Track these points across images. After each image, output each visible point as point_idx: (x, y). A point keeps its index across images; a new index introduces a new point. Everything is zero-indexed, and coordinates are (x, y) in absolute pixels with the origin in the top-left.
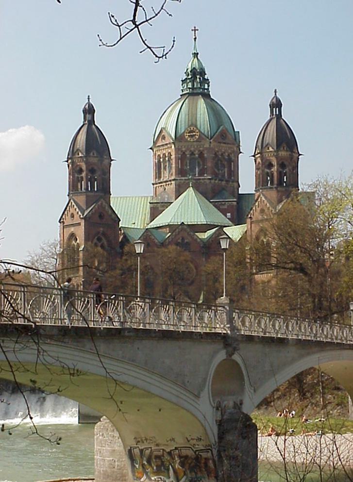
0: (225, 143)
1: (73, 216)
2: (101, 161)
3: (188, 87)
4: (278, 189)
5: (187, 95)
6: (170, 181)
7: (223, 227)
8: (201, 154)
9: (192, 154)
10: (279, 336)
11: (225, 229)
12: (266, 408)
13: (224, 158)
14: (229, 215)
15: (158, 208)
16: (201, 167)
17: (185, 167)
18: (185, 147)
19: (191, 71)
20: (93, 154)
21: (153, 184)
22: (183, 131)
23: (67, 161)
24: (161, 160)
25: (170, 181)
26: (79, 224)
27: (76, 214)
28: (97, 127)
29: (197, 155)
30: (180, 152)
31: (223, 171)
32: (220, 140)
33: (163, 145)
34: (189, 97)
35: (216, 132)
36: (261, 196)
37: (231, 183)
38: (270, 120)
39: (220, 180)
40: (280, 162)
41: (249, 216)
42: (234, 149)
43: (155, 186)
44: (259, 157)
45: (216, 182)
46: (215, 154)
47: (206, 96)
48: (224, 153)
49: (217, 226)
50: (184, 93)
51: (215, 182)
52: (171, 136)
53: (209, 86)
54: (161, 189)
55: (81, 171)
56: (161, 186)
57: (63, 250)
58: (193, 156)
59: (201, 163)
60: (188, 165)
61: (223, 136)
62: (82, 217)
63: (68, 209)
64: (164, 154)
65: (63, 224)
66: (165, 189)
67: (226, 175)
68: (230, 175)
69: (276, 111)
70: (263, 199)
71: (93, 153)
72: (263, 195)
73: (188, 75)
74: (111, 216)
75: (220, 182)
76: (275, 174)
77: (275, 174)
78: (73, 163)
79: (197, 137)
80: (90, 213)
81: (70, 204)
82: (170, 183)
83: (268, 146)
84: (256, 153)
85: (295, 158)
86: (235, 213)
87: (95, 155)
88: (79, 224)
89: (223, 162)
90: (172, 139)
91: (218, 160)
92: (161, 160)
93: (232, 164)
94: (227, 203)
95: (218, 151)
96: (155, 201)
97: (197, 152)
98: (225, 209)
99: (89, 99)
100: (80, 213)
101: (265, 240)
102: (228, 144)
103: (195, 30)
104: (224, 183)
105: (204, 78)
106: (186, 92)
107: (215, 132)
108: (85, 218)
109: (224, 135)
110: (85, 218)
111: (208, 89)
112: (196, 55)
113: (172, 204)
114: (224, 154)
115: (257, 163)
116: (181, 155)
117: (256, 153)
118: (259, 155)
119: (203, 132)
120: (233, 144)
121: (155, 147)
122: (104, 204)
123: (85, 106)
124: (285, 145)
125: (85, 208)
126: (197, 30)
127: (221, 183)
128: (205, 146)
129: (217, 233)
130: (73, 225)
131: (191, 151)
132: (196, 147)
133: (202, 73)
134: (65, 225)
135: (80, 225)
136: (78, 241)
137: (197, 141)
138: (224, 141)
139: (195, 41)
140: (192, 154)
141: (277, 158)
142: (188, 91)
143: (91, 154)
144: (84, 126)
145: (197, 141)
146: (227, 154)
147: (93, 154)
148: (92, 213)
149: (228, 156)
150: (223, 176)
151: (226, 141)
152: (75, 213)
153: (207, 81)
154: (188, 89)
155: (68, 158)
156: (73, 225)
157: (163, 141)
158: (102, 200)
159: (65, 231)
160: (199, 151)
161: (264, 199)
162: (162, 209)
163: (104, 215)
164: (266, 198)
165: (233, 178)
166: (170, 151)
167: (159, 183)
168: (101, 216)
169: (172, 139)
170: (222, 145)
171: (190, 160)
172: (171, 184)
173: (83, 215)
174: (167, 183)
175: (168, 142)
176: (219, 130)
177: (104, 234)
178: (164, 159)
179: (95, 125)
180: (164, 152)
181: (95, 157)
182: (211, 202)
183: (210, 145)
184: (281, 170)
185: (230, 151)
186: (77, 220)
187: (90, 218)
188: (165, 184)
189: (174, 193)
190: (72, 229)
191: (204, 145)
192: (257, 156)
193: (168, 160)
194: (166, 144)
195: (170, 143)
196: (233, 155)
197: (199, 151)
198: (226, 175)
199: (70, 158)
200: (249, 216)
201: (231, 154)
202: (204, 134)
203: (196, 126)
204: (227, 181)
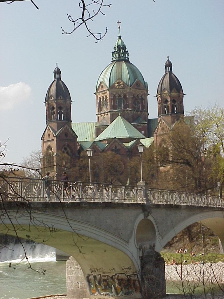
0: (139, 89)
1: (49, 135)
2: (65, 102)
3: (116, 56)
4: (172, 115)
6: (107, 112)
7: (139, 139)
8: (125, 96)
9: (120, 96)
10: (176, 204)
11: (141, 140)
13: (139, 98)
14: (143, 132)
15: (100, 129)
16: (125, 103)
18: (115, 92)
19: (117, 47)
20: (61, 98)
21: (97, 115)
22: (113, 83)
23: (45, 103)
25: (107, 112)
26: (53, 140)
29: (122, 97)
30: (112, 95)
32: (136, 87)
33: (102, 91)
35: (134, 83)
37: (143, 113)
39: (136, 111)
40: (172, 99)
41: (155, 132)
43: (98, 116)
44: (160, 96)
45: (135, 112)
46: (133, 96)
47: (127, 61)
49: (134, 139)
51: (134, 113)
52: (106, 86)
53: (128, 55)
54: (102, 118)
55: (53, 108)
56: (102, 116)
57: (44, 156)
58: (120, 97)
59: (125, 101)
60: (117, 102)
61: (138, 85)
62: (55, 136)
63: (46, 131)
64: (103, 97)
66: (104, 117)
67: (140, 108)
69: (169, 69)
70: (163, 121)
71: (61, 97)
72: (163, 119)
75: (137, 112)
76: (170, 106)
77: (170, 106)
78: (48, 104)
79: (122, 86)
81: (47, 128)
82: (107, 114)
84: (158, 94)
85: (181, 97)
86: (147, 131)
87: (62, 98)
88: (53, 140)
90: (107, 87)
92: (101, 100)
93: (144, 101)
94: (141, 125)
97: (122, 95)
99: (168, 58)
100: (53, 133)
101: (165, 146)
102: (141, 89)
103: (119, 23)
104: (139, 113)
105: (125, 51)
107: (133, 82)
108: (56, 137)
109: (138, 84)
110: (56, 137)
111: (128, 57)
112: (120, 37)
114: (139, 96)
116: (113, 97)
117: (158, 94)
118: (160, 95)
119: (126, 82)
120: (144, 89)
121: (97, 93)
122: (68, 127)
124: (175, 89)
125: (56, 131)
126: (120, 23)
128: (127, 91)
129: (136, 143)
130: (49, 141)
131: (119, 94)
132: (122, 91)
133: (124, 48)
134: (44, 141)
135: (54, 140)
136: (53, 150)
137: (122, 88)
138: (138, 88)
139: (119, 29)
140: (120, 96)
142: (116, 59)
143: (59, 98)
144: (55, 82)
145: (122, 88)
146: (140, 95)
147: (61, 98)
150: (139, 108)
152: (51, 134)
153: (127, 52)
154: (116, 58)
155: (45, 101)
156: (49, 141)
157: (102, 89)
158: (67, 125)
159: (44, 144)
160: (124, 94)
161: (164, 122)
162: (103, 129)
163: (68, 134)
164: (165, 121)
165: (144, 110)
166: (106, 95)
167: (101, 114)
168: (66, 135)
169: (107, 87)
170: (137, 90)
171: (119, 99)
172: (108, 114)
173: (55, 134)
174: (105, 114)
176: (135, 82)
177: (68, 145)
179: (61, 81)
180: (103, 95)
181: (62, 100)
182: (132, 124)
183: (130, 91)
187: (59, 136)
188: (104, 114)
190: (49, 143)
191: (127, 90)
192: (158, 96)
194: (104, 91)
195: (106, 90)
197: (124, 94)
198: (140, 108)
199: (47, 101)
200: (155, 132)
201: (143, 95)
202: (126, 84)
203: (121, 79)
204: (141, 112)
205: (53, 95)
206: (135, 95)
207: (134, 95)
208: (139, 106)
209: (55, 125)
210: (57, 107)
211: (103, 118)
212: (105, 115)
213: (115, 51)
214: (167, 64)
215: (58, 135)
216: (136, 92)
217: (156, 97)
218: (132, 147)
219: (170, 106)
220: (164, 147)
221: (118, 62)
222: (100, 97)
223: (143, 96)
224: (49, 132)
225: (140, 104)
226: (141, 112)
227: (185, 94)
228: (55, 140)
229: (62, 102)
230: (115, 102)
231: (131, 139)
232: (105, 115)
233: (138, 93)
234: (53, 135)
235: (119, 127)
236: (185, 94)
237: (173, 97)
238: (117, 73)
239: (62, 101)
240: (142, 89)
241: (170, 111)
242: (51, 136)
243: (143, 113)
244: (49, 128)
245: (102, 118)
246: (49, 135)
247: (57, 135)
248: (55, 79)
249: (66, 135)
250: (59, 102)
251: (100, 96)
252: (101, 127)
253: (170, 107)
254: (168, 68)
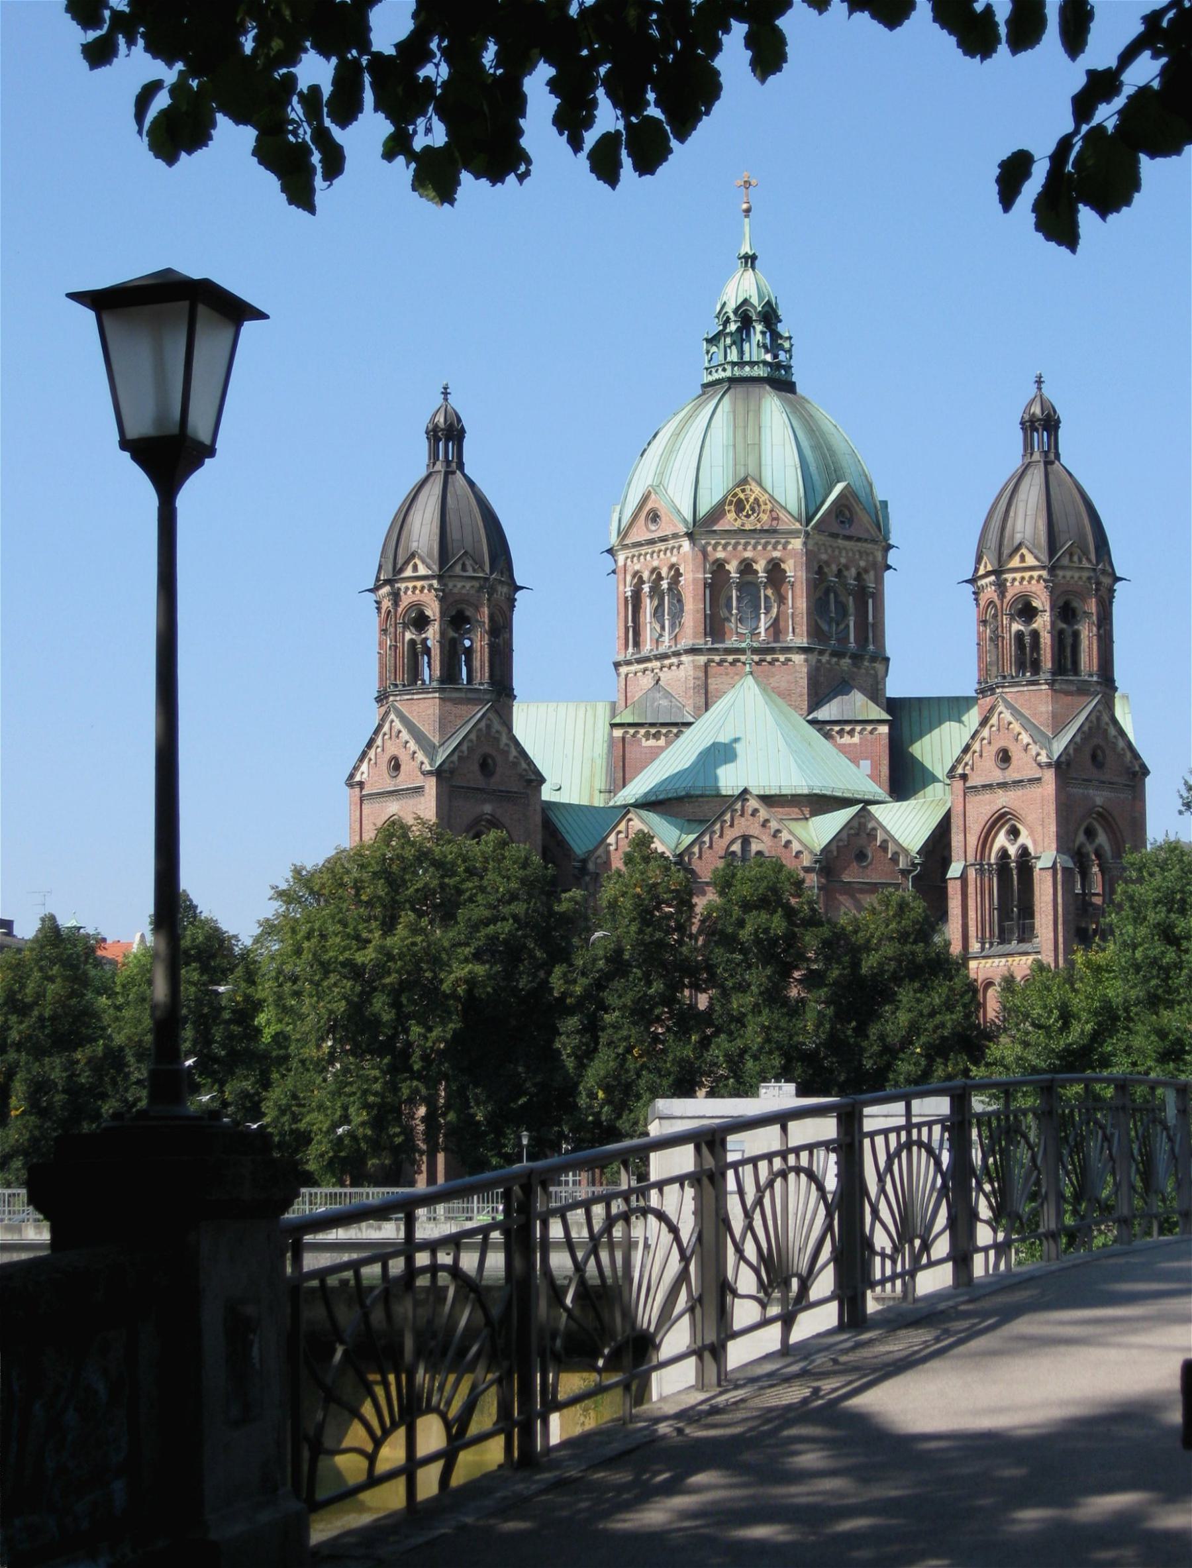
0: (849, 538)
1: (395, 765)
3: (729, 359)
5: (726, 385)
6: (677, 654)
12: (39, 1220)
13: (845, 585)
17: (725, 611)
19: (735, 312)
21: (617, 665)
24: (646, 588)
25: (677, 654)
26: (418, 790)
27: (408, 757)
28: (471, 484)
31: (842, 627)
32: (836, 528)
33: (651, 542)
34: (732, 391)
36: (1001, 708)
37: (866, 663)
38: (1026, 467)
39: (835, 654)
40: (1061, 603)
42: (875, 557)
43: (624, 670)
45: (825, 658)
48: (847, 567)
49: (844, 802)
50: (715, 376)
54: (645, 680)
55: (421, 622)
56: (645, 670)
58: (749, 578)
61: (843, 515)
62: (427, 767)
63: (379, 742)
64: (747, 567)
65: (362, 789)
66: (659, 680)
67: (852, 639)
68: (863, 640)
70: (1007, 716)
72: (1009, 706)
73: (727, 321)
74: (515, 764)
75: (834, 660)
77: (1046, 639)
80: (455, 758)
81: (386, 728)
82: (674, 660)
83: (1024, 551)
84: (981, 572)
88: (418, 790)
89: (843, 599)
90: (685, 521)
91: (827, 591)
93: (870, 601)
95: (827, 563)
96: (630, 720)
98: (856, 744)
100: (420, 756)
102: (859, 540)
106: (721, 375)
108: (439, 773)
109: (847, 513)
110: (439, 773)
113: (688, 732)
114: (846, 573)
115: (982, 603)
118: (992, 578)
120: (874, 541)
121: (626, 547)
123: (435, 415)
125: (436, 741)
127: (837, 664)
134: (364, 793)
136: (1024, 839)
138: (847, 533)
141: (442, 600)
142: (728, 374)
144: (432, 480)
146: (853, 571)
148: (460, 758)
149: (855, 580)
150: (844, 640)
151: (853, 531)
152: (404, 758)
154: (728, 368)
155: (378, 579)
157: (653, 528)
159: (365, 812)
161: (1011, 719)
163: (495, 765)
164: (1016, 712)
165: (871, 647)
166: (674, 560)
167: (639, 661)
168: (486, 766)
171: (741, 587)
173: (432, 761)
174: (667, 662)
175: (668, 533)
178: (655, 590)
179: (465, 475)
180: (655, 563)
184: (452, 634)
185: (862, 564)
186: (409, 776)
187: (452, 772)
188: (657, 664)
189: (806, 697)
193: (670, 589)
194: (663, 539)
195: (675, 536)
196: (872, 573)
198: (852, 639)
199: (388, 582)
201: (866, 571)
204: (857, 658)
205: (423, 551)
206: (826, 570)
207: (820, 568)
208: (848, 626)
209: (430, 711)
210: (443, 613)
211: (653, 683)
212: (661, 669)
213: (719, 334)
214: (436, 425)
215: (446, 767)
216: (837, 553)
217: (970, 588)
218: (834, 843)
219: (1048, 636)
220: (1004, 854)
221: (739, 390)
222: (636, 573)
223: (865, 577)
224: (392, 749)
225: (852, 619)
226: (857, 658)
227: (522, 588)
228: (431, 785)
229: (473, 592)
230: (722, 601)
231: (821, 803)
232: (661, 669)
233: (843, 560)
234: (417, 764)
235: (694, 740)
236: (522, 588)
237: (1066, 592)
238: (734, 446)
239: (468, 585)
240: (866, 540)
241: (1049, 665)
242: (402, 768)
243: (866, 663)
244: (398, 725)
245: (646, 681)
246: (395, 765)
247: (441, 765)
248: (434, 464)
249: (486, 766)
250: (456, 591)
251: (637, 567)
252: (642, 731)
253: (1048, 641)
254: (441, 444)
